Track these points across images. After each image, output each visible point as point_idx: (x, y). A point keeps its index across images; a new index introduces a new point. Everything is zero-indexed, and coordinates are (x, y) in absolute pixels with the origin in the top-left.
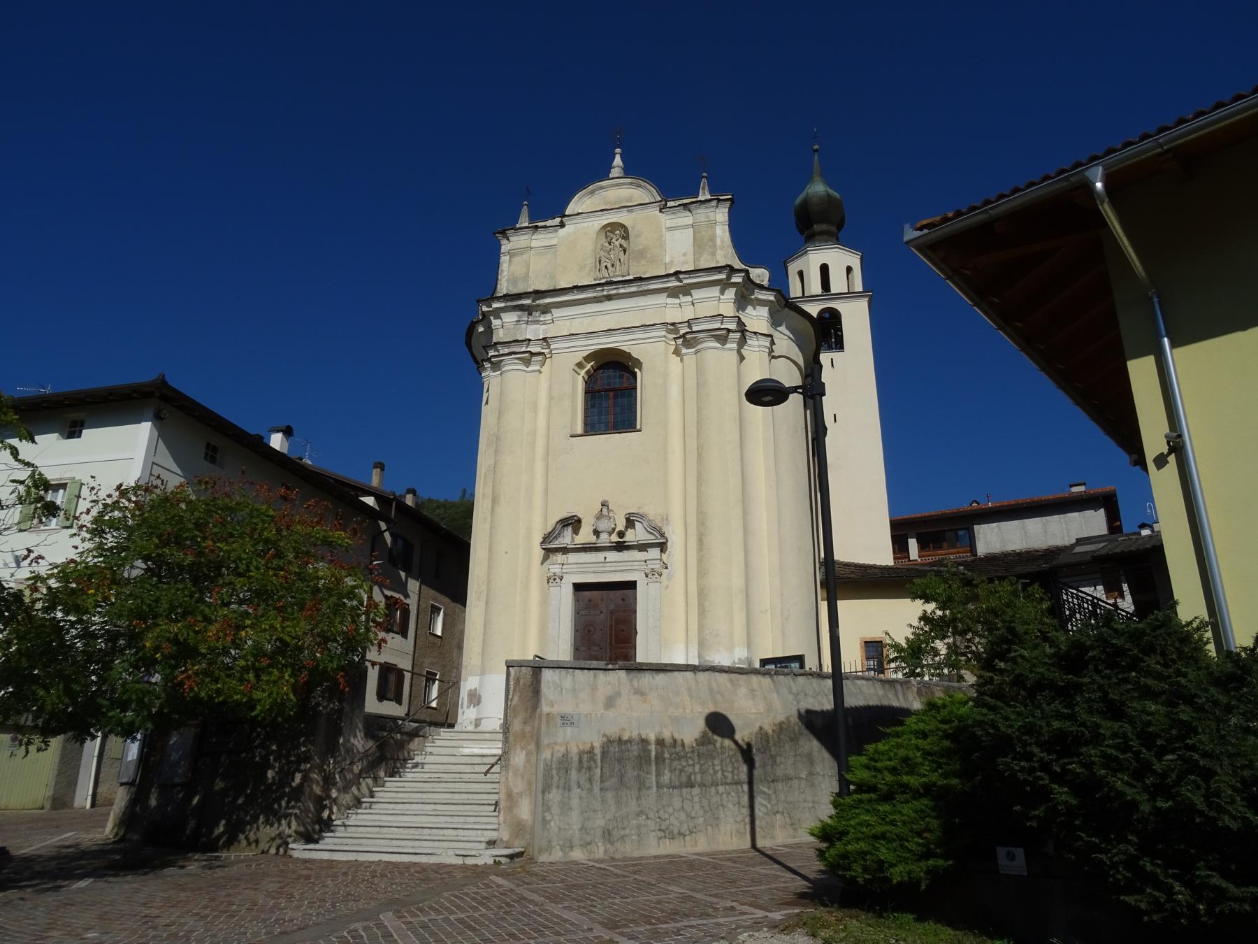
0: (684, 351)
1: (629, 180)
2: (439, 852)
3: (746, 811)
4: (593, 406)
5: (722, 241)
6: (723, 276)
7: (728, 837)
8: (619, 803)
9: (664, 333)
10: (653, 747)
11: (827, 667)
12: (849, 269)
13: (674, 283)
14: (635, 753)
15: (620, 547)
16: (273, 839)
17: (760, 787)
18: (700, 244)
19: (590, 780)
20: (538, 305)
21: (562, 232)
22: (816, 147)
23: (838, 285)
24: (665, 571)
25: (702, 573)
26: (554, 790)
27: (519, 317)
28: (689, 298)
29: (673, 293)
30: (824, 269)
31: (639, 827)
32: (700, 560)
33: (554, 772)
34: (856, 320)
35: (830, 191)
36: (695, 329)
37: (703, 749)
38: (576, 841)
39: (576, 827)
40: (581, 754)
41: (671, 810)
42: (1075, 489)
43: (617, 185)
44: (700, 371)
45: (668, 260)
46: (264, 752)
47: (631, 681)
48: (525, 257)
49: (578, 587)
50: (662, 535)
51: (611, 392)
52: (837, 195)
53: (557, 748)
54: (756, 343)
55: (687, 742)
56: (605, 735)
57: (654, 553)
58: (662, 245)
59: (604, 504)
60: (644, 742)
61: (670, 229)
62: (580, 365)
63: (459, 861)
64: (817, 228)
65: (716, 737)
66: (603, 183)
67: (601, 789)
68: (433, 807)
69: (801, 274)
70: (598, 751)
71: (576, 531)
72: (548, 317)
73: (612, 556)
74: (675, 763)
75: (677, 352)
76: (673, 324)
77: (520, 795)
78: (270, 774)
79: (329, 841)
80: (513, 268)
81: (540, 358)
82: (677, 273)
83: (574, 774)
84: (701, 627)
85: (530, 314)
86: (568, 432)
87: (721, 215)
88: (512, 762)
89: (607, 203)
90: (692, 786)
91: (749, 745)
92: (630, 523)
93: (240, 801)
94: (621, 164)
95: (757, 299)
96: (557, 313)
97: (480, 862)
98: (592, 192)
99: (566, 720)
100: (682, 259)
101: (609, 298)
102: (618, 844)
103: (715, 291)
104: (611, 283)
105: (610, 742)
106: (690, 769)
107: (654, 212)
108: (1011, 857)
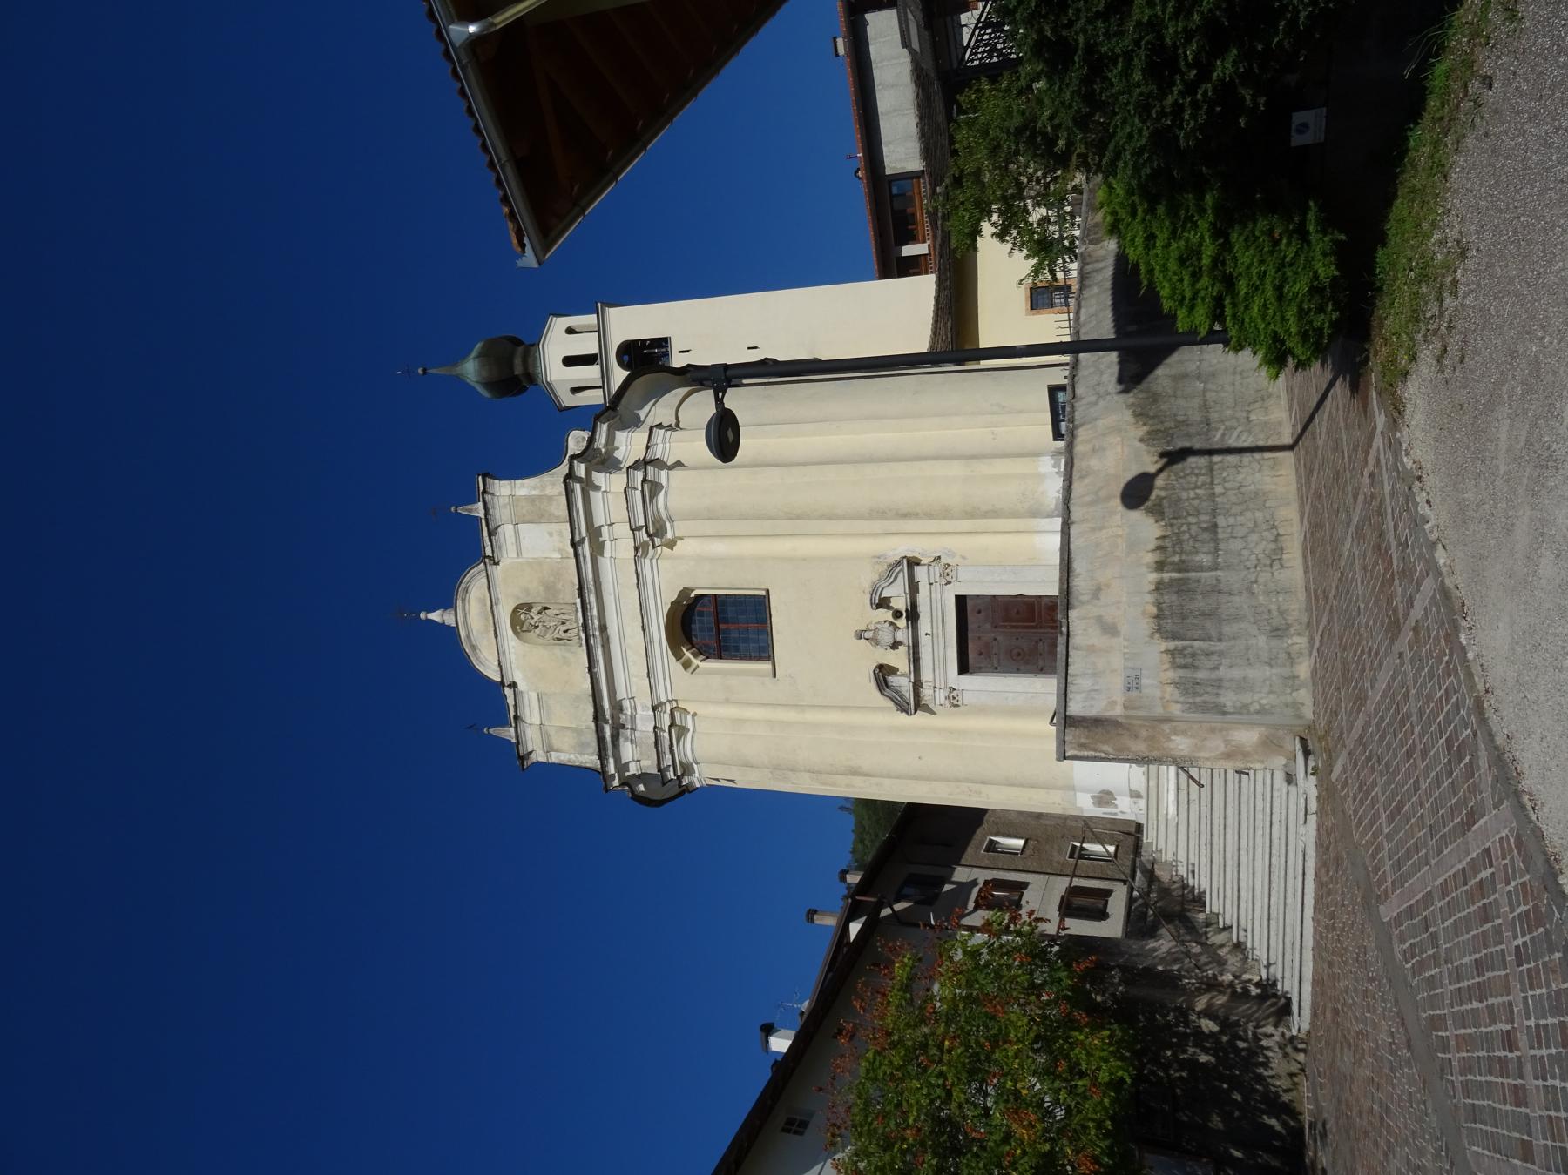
0: (669, 535)
1: (459, 603)
2: (1301, 845)
3: (1247, 458)
4: (737, 649)
5: (535, 488)
6: (578, 487)
7: (1279, 480)
8: (1238, 618)
9: (647, 561)
10: (1166, 576)
11: (1066, 358)
12: (570, 331)
13: (586, 549)
14: (1174, 597)
15: (913, 615)
16: (1286, 1055)
17: (1216, 440)
18: (539, 517)
19: (1208, 654)
20: (612, 716)
21: (522, 686)
22: (420, 371)
23: (588, 345)
24: (943, 560)
25: (945, 514)
26: (1222, 699)
27: (626, 739)
28: (605, 530)
29: (598, 549)
30: (570, 361)
31: (1268, 593)
32: (930, 516)
33: (1198, 699)
34: (632, 322)
35: (474, 353)
36: (642, 522)
37: (1168, 512)
38: (1286, 671)
39: (1268, 671)
40: (1175, 666)
41: (1245, 553)
42: (841, 50)
43: (465, 617)
44: (693, 516)
45: (557, 555)
46: (1175, 1066)
47: (1082, 603)
48: (552, 732)
49: (964, 668)
50: (898, 563)
51: (719, 626)
52: (479, 346)
53: (1167, 697)
54: (660, 446)
55: (1159, 533)
56: (1152, 636)
57: (920, 573)
58: (539, 563)
59: (860, 635)
60: (1159, 587)
61: (519, 553)
62: (687, 665)
63: (1313, 819)
64: (518, 371)
65: (1153, 497)
66: (463, 634)
67: (1220, 640)
68: (1243, 852)
69: (575, 390)
70: (1172, 645)
71: (893, 671)
72: (626, 704)
73: (924, 625)
74: (1187, 547)
75: (671, 545)
76: (636, 549)
77: (1227, 742)
78: (1203, 1058)
79: (1288, 985)
80: (566, 747)
81: (677, 714)
82: (573, 544)
83: (1201, 675)
84: (1014, 514)
85: (623, 727)
86: (769, 680)
87: (502, 489)
88: (1185, 753)
89: (487, 631)
90: (1215, 526)
91: (1162, 455)
92: (883, 603)
93: (1238, 1097)
94: (438, 612)
95: (606, 445)
96: (621, 693)
97: (1313, 793)
98: (474, 648)
99: (1132, 685)
100: (556, 537)
101: (603, 628)
102: (1290, 619)
103: (596, 497)
104: (585, 626)
105: (1159, 630)
106: (1194, 529)
107: (497, 572)
108: (1303, 128)
